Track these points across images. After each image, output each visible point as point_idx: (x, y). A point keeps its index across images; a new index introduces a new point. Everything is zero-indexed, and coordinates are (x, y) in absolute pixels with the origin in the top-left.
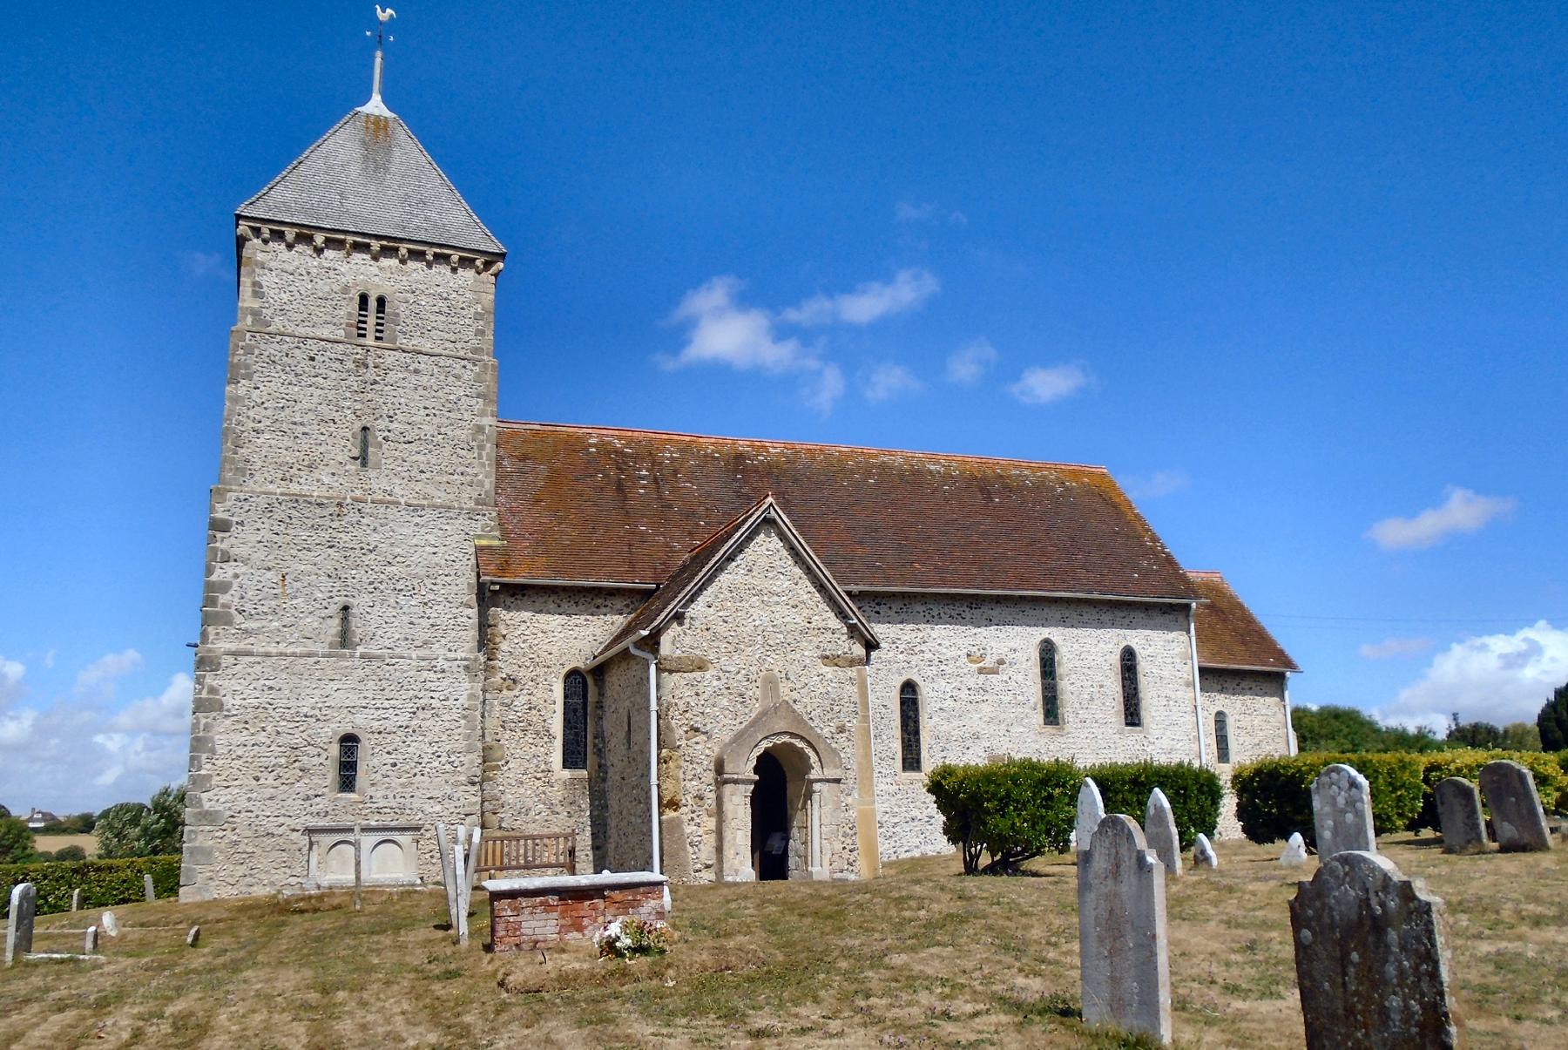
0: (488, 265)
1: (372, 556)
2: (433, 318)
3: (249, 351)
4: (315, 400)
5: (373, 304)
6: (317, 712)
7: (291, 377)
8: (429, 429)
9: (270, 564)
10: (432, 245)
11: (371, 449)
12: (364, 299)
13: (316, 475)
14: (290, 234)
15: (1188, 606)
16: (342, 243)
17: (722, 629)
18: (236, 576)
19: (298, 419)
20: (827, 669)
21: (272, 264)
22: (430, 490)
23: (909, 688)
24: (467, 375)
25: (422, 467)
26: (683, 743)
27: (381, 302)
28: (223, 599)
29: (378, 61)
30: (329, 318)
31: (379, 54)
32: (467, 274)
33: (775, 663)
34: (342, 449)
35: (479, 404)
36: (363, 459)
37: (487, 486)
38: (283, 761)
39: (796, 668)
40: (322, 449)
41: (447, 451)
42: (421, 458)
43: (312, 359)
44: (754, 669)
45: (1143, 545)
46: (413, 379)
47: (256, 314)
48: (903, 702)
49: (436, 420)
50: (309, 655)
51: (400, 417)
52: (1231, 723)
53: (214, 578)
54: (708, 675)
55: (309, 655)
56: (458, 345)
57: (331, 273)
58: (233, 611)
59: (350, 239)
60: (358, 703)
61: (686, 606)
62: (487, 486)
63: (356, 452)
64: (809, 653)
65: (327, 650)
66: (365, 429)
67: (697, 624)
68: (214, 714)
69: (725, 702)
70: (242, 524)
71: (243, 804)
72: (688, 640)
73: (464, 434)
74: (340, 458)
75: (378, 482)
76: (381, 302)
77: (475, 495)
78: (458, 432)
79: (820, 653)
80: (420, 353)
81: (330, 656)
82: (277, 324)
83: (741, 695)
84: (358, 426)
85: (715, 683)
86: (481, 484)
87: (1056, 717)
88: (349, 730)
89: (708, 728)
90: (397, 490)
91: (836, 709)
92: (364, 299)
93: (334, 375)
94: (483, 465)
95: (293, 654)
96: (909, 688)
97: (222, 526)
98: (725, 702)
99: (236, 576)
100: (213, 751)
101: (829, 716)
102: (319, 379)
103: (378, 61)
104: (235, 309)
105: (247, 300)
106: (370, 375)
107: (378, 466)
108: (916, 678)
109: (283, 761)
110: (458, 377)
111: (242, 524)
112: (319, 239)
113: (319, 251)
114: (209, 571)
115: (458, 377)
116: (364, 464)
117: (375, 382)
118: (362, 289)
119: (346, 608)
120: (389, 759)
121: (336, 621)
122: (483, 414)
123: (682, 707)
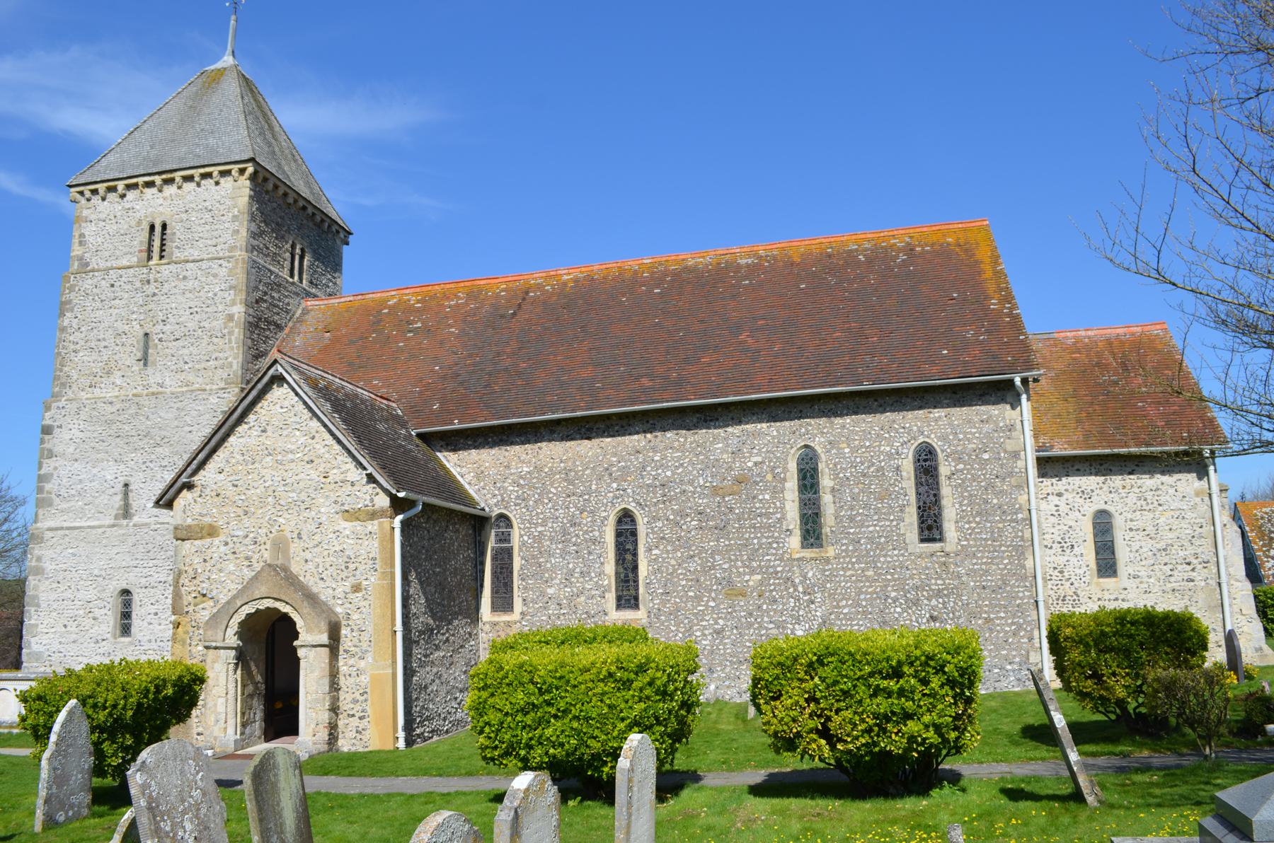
0: (242, 171)
1: (146, 440)
2: (200, 229)
3: (72, 289)
4: (113, 318)
5: (158, 229)
6: (103, 573)
7: (99, 304)
8: (191, 325)
9: (77, 456)
10: (160, 173)
11: (150, 351)
12: (152, 227)
13: (112, 379)
14: (101, 187)
15: (1011, 381)
16: (135, 186)
17: (230, 492)
18: (56, 468)
19: (101, 337)
20: (347, 524)
21: (93, 217)
22: (191, 378)
23: (626, 518)
24: (223, 272)
25: (186, 358)
26: (191, 608)
27: (164, 226)
28: (48, 487)
29: (232, 22)
30: (128, 249)
31: (233, 17)
32: (227, 183)
33: (288, 522)
34: (129, 357)
35: (230, 295)
36: (145, 360)
37: (235, 367)
38: (81, 612)
39: (311, 527)
40: (116, 357)
41: (206, 339)
42: (186, 351)
43: (112, 286)
44: (264, 531)
45: (986, 309)
46: (182, 285)
47: (81, 259)
48: (619, 534)
49: (197, 317)
50: (100, 527)
51: (171, 320)
52: (1119, 523)
53: (42, 472)
54: (216, 541)
55: (100, 527)
56: (219, 248)
57: (130, 213)
58: (53, 496)
59: (141, 180)
60: (131, 563)
61: (195, 472)
62: (235, 367)
63: (139, 355)
64: (325, 508)
65: (112, 522)
66: (146, 334)
67: (208, 491)
68: (38, 577)
69: (231, 567)
70: (60, 427)
71: (56, 646)
72: (197, 509)
73: (218, 324)
74: (128, 363)
75: (154, 376)
76: (164, 226)
77: (225, 376)
78: (215, 323)
79: (338, 508)
80: (187, 261)
81: (113, 526)
82: (93, 265)
83: (247, 558)
84: (141, 333)
85: (223, 549)
86: (231, 365)
87: (818, 537)
88: (125, 586)
89: (214, 593)
90: (168, 382)
91: (352, 566)
92: (152, 227)
93: (126, 296)
94: (232, 348)
95: (90, 527)
96: (626, 518)
97: (47, 430)
98: (231, 567)
99: (56, 468)
100: (38, 605)
101: (344, 575)
102: (117, 301)
103: (232, 22)
104: (69, 257)
105: (77, 250)
106: (151, 289)
107: (154, 363)
108: (632, 507)
109: (81, 612)
110: (215, 276)
111: (60, 427)
112: (121, 186)
113: (123, 196)
114: (40, 466)
115: (215, 276)
116: (145, 365)
117: (154, 295)
118: (150, 219)
119: (126, 485)
120: (153, 609)
121: (120, 497)
122: (233, 303)
123: (191, 574)
